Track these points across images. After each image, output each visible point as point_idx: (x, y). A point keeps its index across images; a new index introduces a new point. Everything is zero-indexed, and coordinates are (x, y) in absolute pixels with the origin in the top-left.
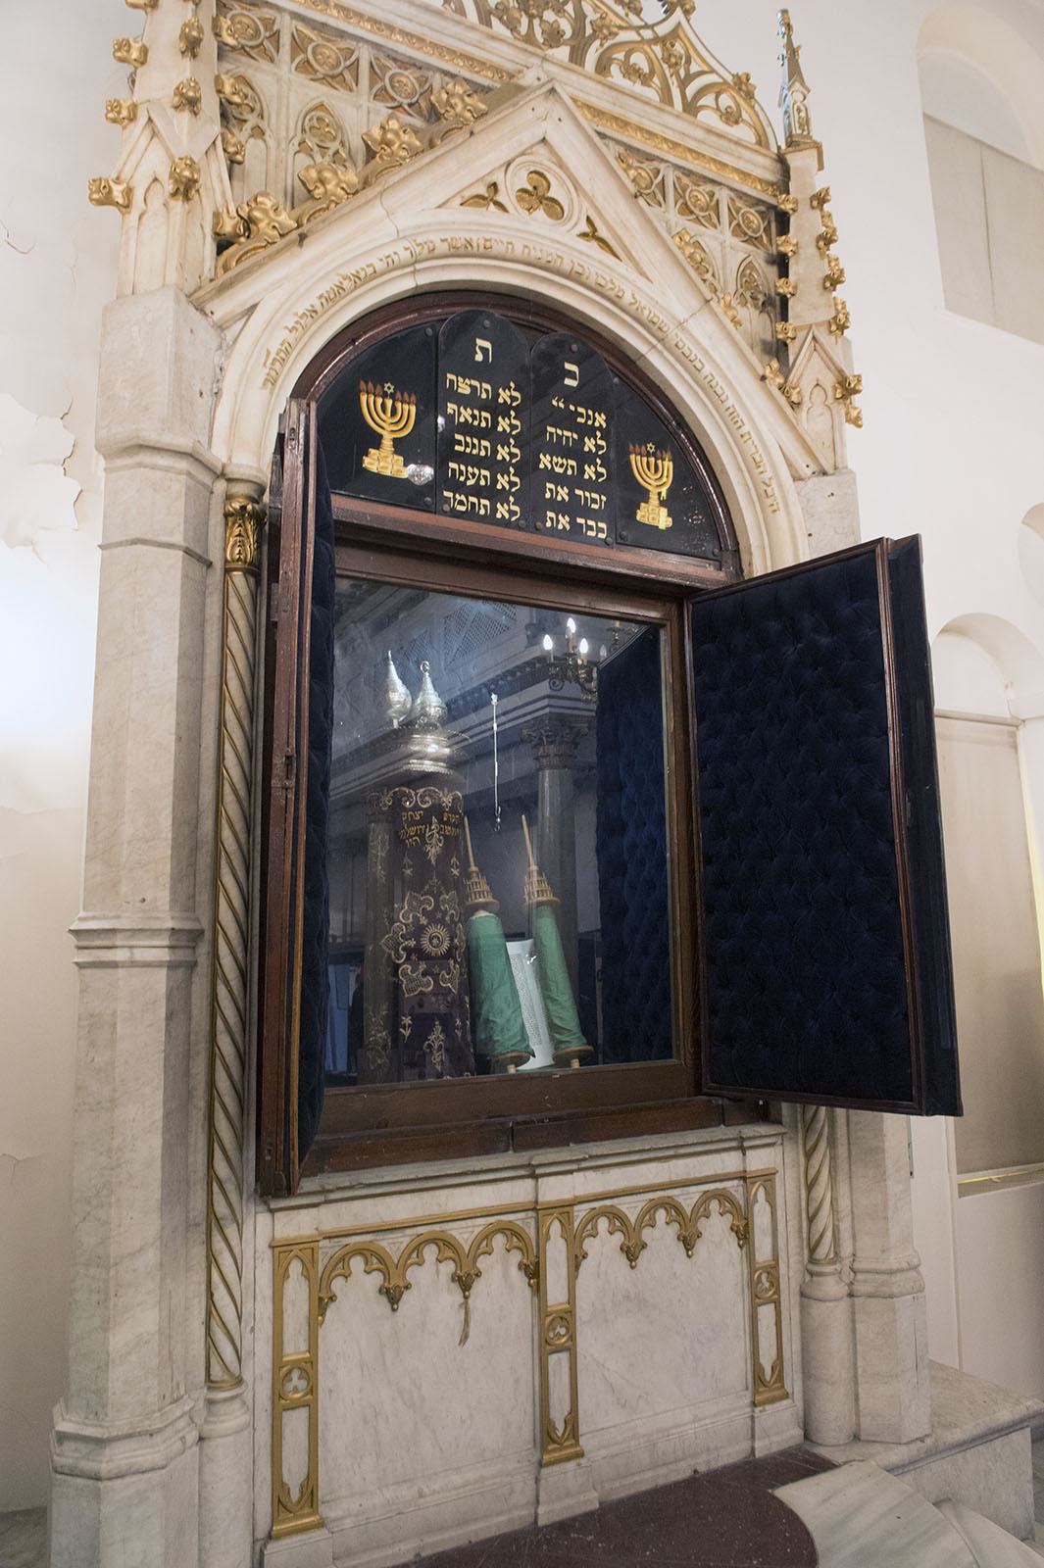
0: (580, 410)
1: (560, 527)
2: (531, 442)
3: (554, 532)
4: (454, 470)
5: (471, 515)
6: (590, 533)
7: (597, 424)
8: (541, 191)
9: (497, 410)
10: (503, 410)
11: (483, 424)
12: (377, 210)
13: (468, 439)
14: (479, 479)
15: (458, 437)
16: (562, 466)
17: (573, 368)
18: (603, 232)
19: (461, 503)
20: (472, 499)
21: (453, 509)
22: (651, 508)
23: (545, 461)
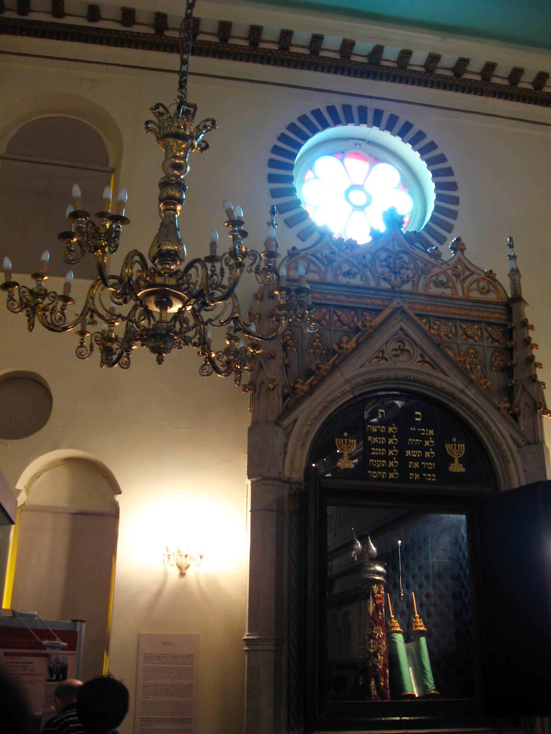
0: (423, 430)
1: (416, 478)
2: (402, 446)
3: (413, 481)
4: (371, 462)
5: (379, 479)
6: (429, 479)
7: (430, 434)
8: (402, 347)
9: (388, 436)
10: (390, 436)
11: (383, 442)
12: (338, 374)
13: (377, 449)
14: (382, 464)
15: (373, 449)
16: (415, 454)
17: (379, 568)
18: (427, 359)
19: (375, 475)
20: (379, 473)
21: (372, 478)
22: (455, 465)
23: (408, 453)
